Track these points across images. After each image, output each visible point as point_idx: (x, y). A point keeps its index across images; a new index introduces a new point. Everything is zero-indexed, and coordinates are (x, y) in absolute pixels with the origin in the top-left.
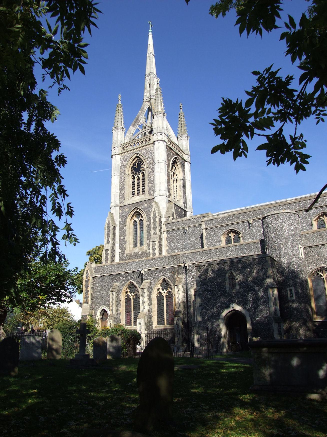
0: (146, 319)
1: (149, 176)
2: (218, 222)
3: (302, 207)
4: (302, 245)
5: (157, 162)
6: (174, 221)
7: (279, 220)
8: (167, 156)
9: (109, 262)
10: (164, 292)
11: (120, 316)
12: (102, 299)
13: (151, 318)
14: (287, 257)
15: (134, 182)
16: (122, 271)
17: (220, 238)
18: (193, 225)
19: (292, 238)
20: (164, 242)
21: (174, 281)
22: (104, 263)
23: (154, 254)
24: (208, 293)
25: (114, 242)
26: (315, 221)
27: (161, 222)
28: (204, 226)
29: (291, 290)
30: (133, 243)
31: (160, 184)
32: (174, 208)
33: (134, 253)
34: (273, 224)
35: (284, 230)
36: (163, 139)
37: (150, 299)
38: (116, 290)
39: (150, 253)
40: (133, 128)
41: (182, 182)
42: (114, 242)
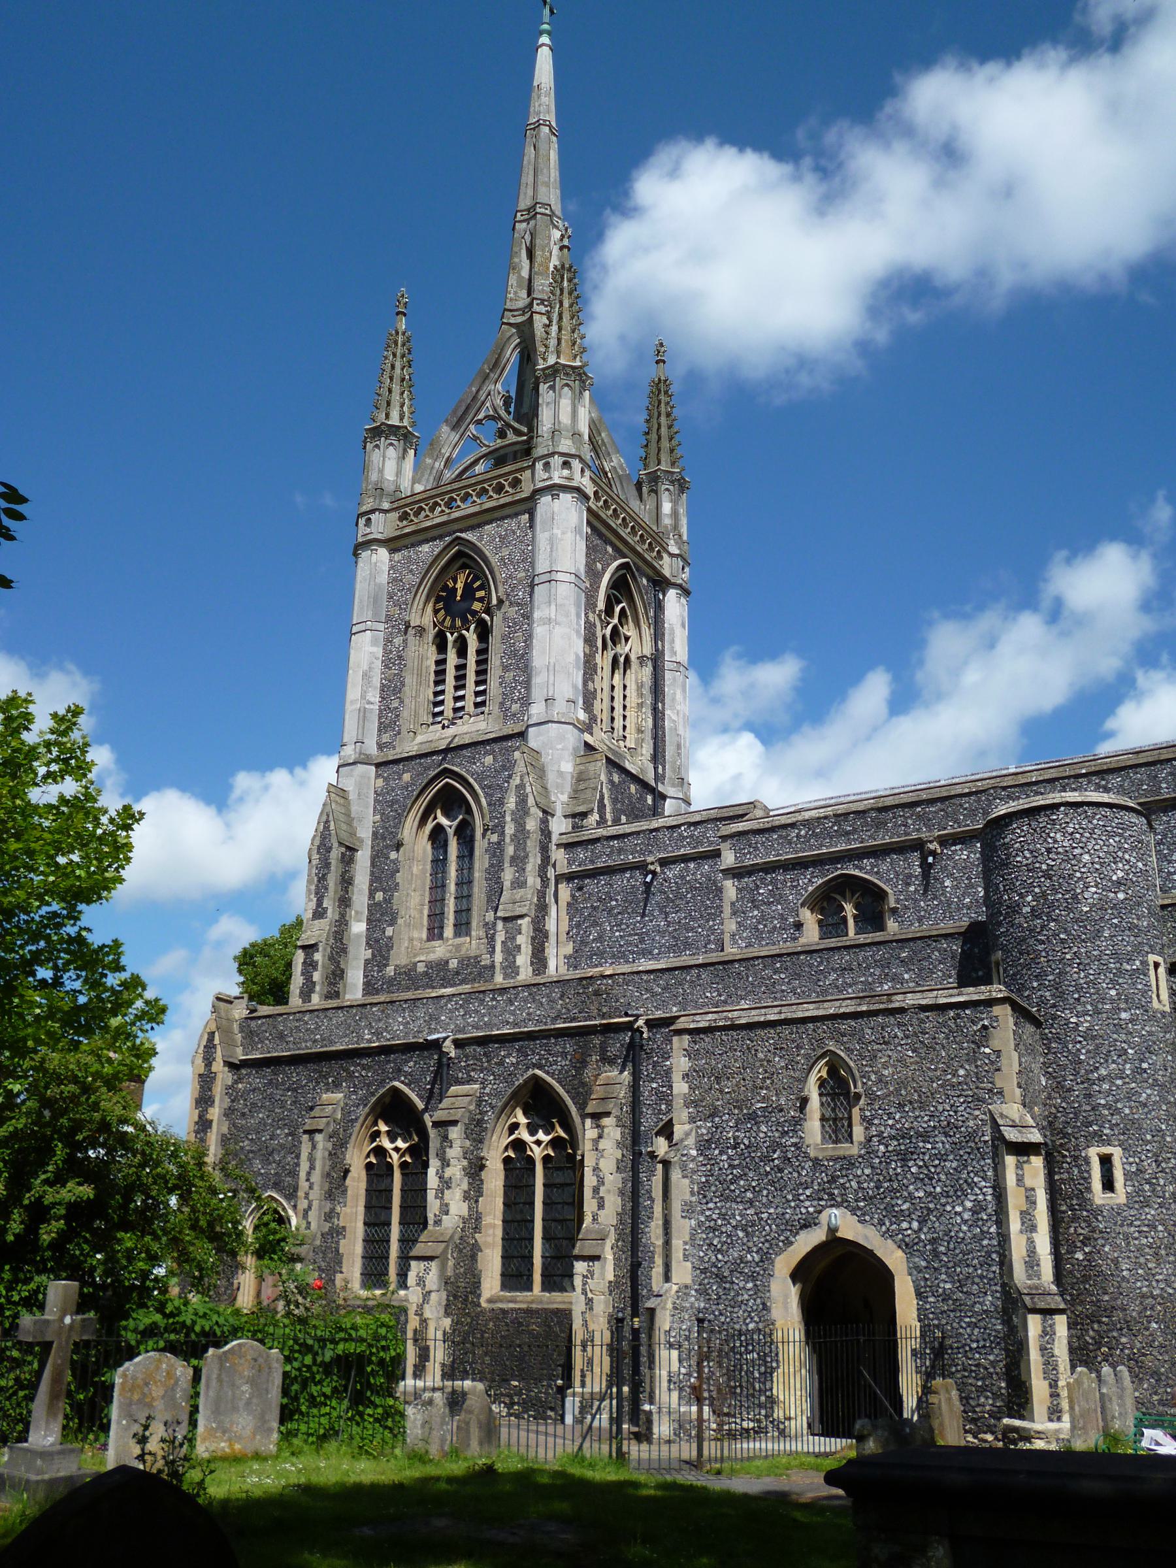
0: (451, 1263)
1: (505, 638)
2: (790, 843)
3: (1164, 785)
4: (1160, 954)
6: (602, 832)
7: (1059, 836)
8: (588, 555)
9: (316, 999)
10: (538, 1143)
11: (342, 1242)
12: (266, 1162)
13: (473, 1258)
14: (1089, 1007)
15: (441, 662)
16: (360, 1038)
18: (682, 851)
19: (1115, 921)
21: (582, 1095)
22: (295, 1001)
23: (511, 969)
24: (724, 1157)
25: (343, 915)
27: (546, 833)
28: (729, 858)
29: (1106, 1161)
30: (425, 923)
31: (551, 673)
32: (603, 778)
33: (429, 965)
34: (1027, 854)
36: (574, 484)
37: (476, 1168)
38: (328, 1124)
39: (493, 966)
40: (454, 433)
41: (648, 670)
42: (343, 915)
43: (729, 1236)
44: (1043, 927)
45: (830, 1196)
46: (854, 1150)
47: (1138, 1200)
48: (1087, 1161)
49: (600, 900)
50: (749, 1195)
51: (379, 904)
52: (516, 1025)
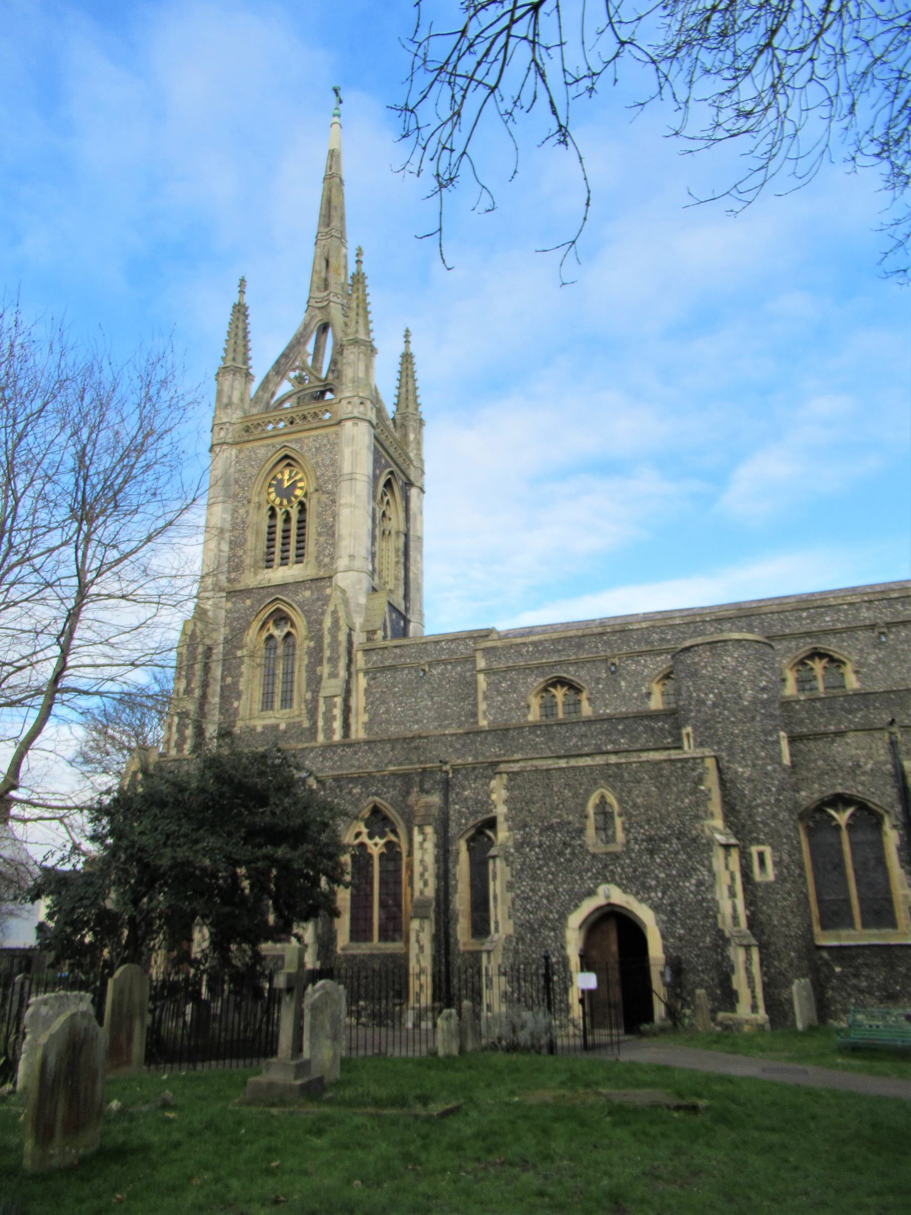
5: (346, 477)
10: (376, 844)
17: (524, 698)
20: (359, 701)
23: (329, 731)
24: (533, 853)
26: (536, 696)
27: (350, 643)
28: (481, 663)
34: (709, 669)
35: (743, 685)
36: (368, 418)
43: (537, 903)
44: (720, 713)
45: (604, 877)
46: (617, 848)
47: (780, 878)
48: (750, 855)
49: (387, 687)
50: (550, 876)
51: (228, 686)
52: (359, 767)
